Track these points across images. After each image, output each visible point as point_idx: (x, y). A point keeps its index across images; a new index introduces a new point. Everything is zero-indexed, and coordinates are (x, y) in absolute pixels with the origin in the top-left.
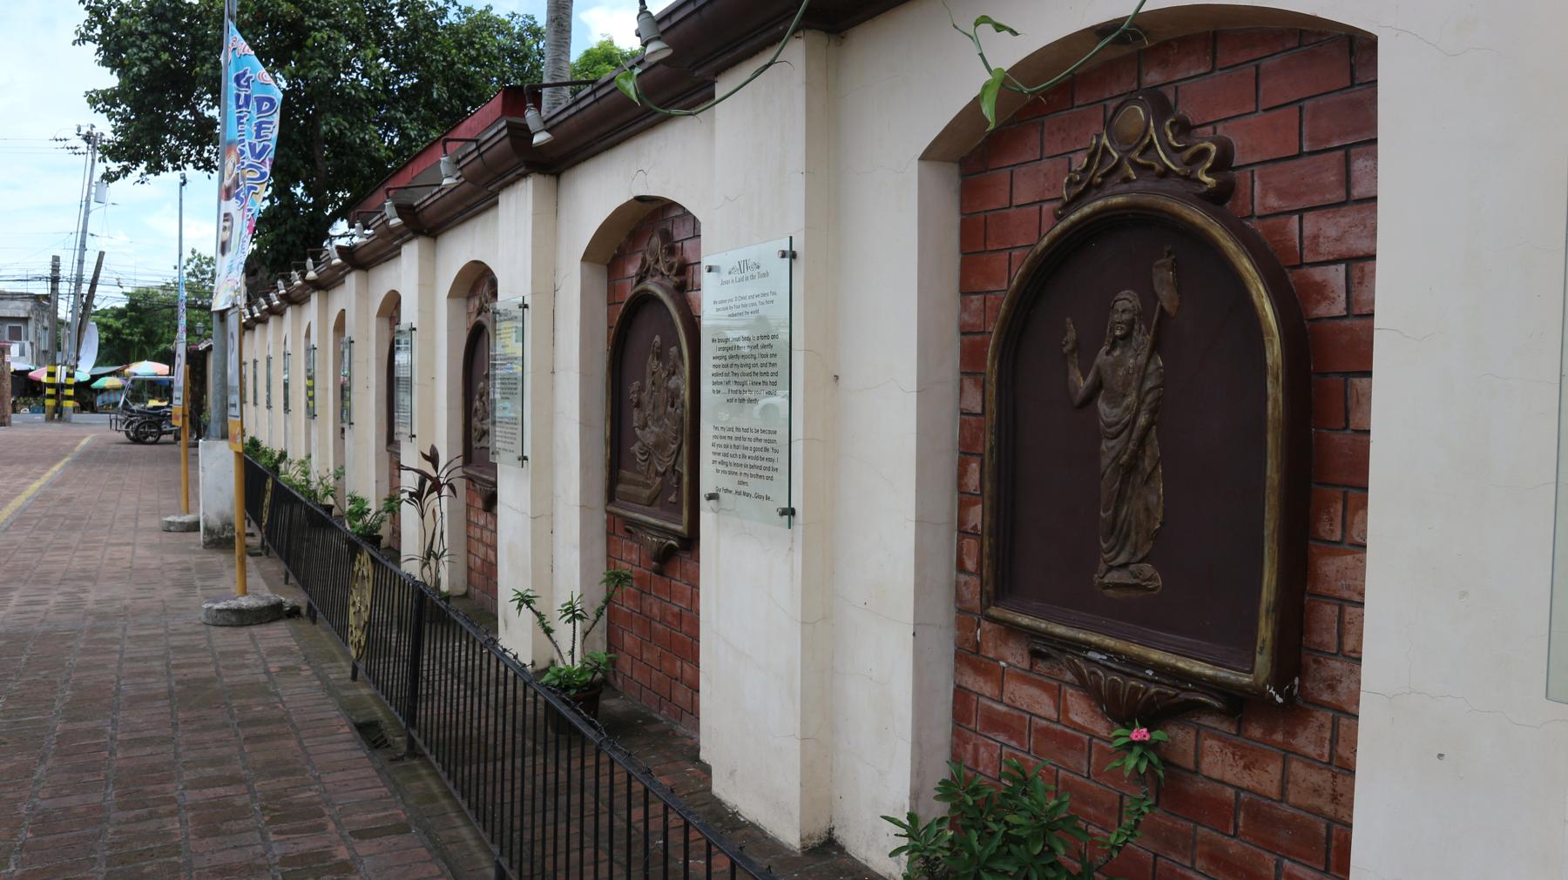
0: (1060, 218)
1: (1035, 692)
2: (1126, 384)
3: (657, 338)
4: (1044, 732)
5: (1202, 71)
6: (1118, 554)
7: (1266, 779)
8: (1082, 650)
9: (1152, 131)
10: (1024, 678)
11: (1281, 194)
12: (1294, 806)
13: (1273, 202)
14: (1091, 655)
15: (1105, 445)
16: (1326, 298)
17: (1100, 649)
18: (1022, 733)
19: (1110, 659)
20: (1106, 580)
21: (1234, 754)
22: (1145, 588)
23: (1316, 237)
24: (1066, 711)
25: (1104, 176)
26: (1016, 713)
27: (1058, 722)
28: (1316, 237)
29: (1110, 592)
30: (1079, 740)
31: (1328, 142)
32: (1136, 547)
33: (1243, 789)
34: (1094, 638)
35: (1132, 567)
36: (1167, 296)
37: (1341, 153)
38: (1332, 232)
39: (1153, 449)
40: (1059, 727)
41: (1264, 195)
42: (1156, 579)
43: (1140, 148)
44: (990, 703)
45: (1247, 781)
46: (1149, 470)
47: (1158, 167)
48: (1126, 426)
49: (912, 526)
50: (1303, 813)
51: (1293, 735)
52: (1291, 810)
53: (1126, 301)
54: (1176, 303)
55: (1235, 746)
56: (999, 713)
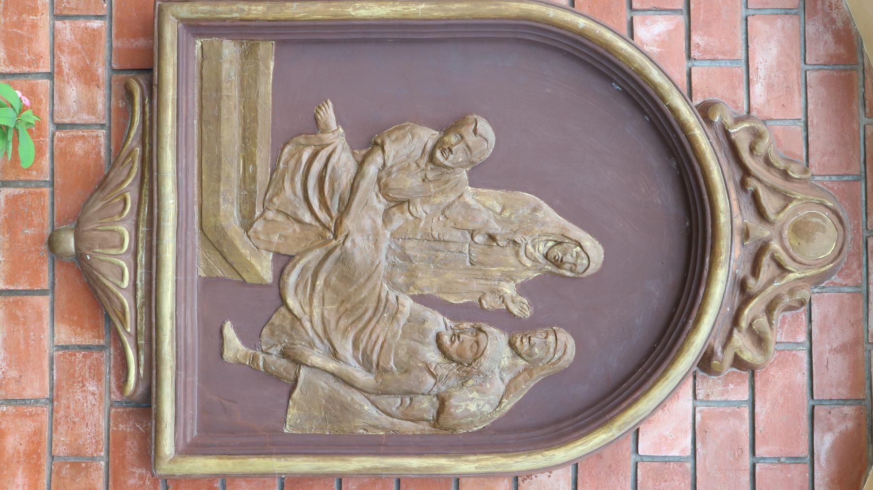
0: (705, 111)
39: (448, 321)
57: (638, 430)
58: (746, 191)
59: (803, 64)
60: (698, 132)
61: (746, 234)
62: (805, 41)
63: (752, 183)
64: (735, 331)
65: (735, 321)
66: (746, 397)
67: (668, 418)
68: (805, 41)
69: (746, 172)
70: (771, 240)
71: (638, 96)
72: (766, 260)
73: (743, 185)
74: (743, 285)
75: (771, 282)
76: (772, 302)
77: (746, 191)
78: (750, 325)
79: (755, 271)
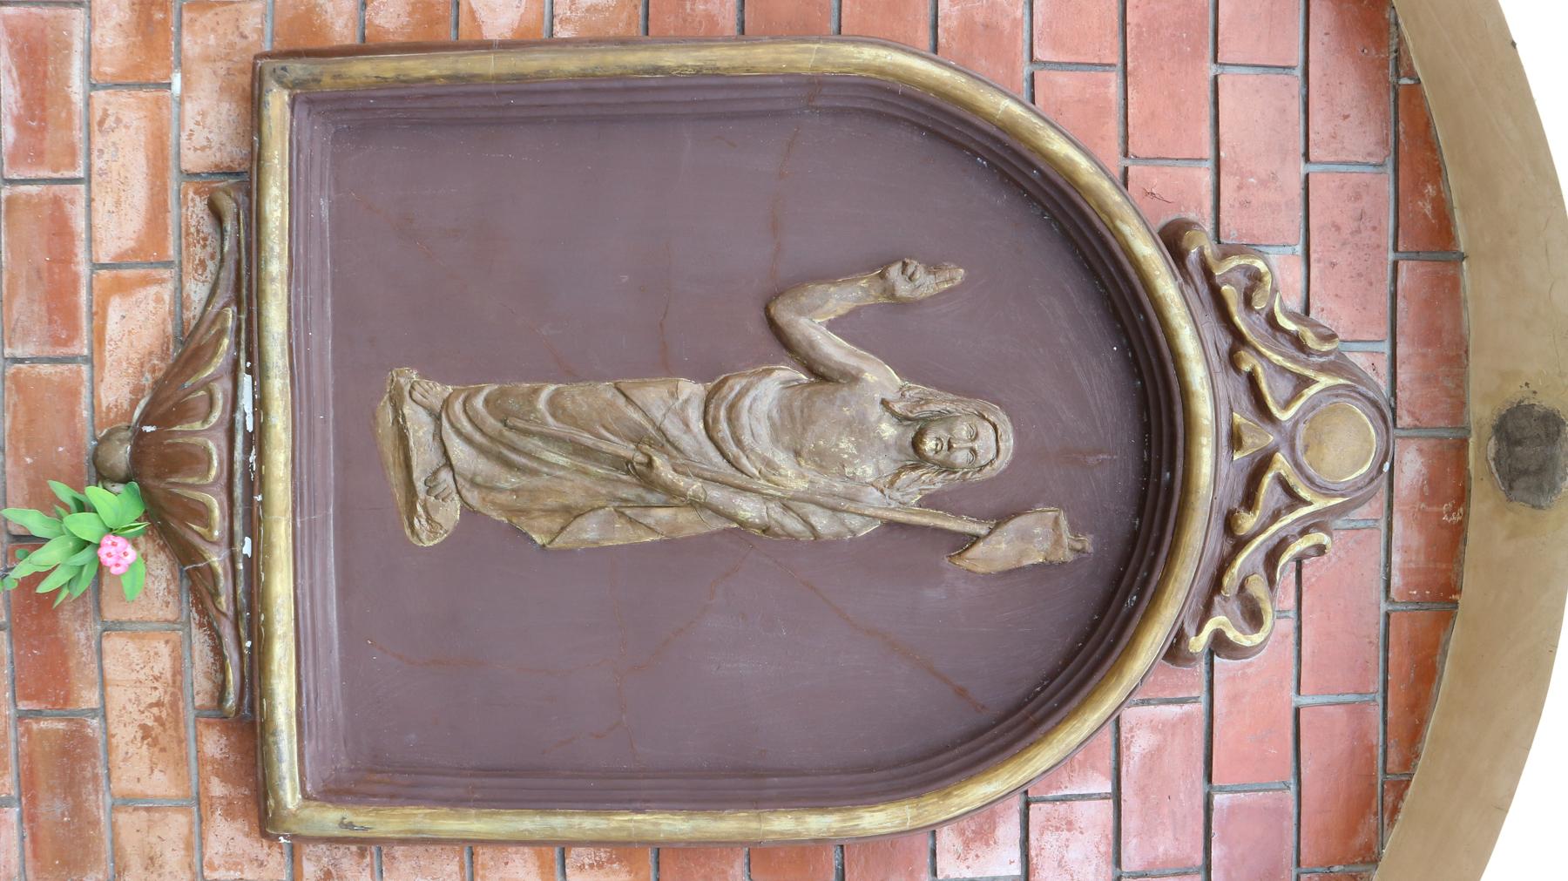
0: (1173, 240)
1: (139, 193)
2: (824, 460)
3: (626, 278)
4: (60, 230)
5: (1396, 580)
6: (468, 440)
7: (136, 769)
8: (249, 358)
9: (1320, 504)
10: (160, 154)
11: (1153, 757)
12: (113, 825)
13: (1139, 744)
14: (246, 381)
15: (691, 390)
16: (967, 845)
17: (261, 405)
18: (39, 157)
19: (248, 437)
20: (408, 409)
21: (159, 704)
22: (412, 511)
23: (1070, 825)
24: (122, 287)
25: (1252, 379)
26: (79, 135)
27: (97, 266)
28: (1070, 825)
29: (389, 416)
30: (73, 329)
31: (1222, 839)
32: (486, 487)
33: (105, 717)
34: (278, 384)
35: (445, 475)
36: (1000, 550)
37: (1199, 859)
38: (1074, 854)
39: (688, 523)
40: (83, 269)
41: (1156, 727)
42: (433, 533)
43: (1293, 480)
44: (78, 46)
45: (124, 734)
46: (649, 521)
47: (1248, 522)
48: (733, 464)
49: (1535, 95)
50: (108, 845)
51: (229, 814)
52: (103, 817)
53: (986, 442)
54: (981, 568)
55: (174, 704)
56: (65, 81)
57: (1118, 720)
58: (1237, 370)
59: (1293, 693)
60: (1167, 286)
61: (1236, 440)
62: (1299, 629)
63: (1248, 362)
64: (1217, 599)
65: (1216, 585)
66: (1108, 788)
67: (1142, 710)
68: (1299, 629)
69: (1238, 339)
70: (1277, 450)
71: (1071, 226)
72: (1268, 480)
73: (1233, 362)
74: (1229, 524)
75: (1276, 516)
76: (1261, 461)
77: (1237, 370)
78: (1242, 587)
79: (1249, 501)
